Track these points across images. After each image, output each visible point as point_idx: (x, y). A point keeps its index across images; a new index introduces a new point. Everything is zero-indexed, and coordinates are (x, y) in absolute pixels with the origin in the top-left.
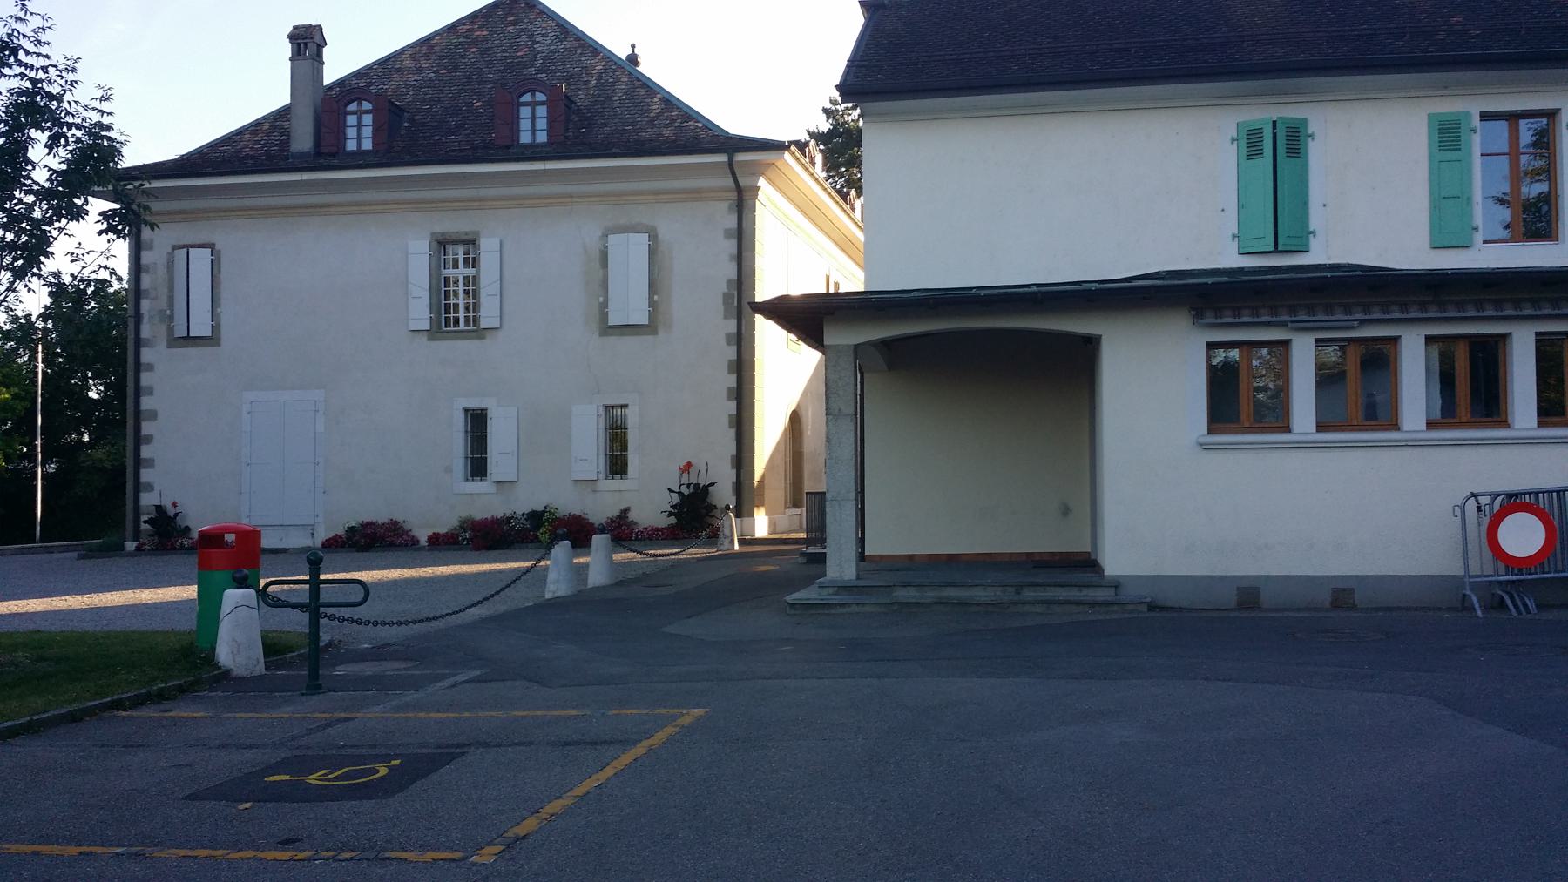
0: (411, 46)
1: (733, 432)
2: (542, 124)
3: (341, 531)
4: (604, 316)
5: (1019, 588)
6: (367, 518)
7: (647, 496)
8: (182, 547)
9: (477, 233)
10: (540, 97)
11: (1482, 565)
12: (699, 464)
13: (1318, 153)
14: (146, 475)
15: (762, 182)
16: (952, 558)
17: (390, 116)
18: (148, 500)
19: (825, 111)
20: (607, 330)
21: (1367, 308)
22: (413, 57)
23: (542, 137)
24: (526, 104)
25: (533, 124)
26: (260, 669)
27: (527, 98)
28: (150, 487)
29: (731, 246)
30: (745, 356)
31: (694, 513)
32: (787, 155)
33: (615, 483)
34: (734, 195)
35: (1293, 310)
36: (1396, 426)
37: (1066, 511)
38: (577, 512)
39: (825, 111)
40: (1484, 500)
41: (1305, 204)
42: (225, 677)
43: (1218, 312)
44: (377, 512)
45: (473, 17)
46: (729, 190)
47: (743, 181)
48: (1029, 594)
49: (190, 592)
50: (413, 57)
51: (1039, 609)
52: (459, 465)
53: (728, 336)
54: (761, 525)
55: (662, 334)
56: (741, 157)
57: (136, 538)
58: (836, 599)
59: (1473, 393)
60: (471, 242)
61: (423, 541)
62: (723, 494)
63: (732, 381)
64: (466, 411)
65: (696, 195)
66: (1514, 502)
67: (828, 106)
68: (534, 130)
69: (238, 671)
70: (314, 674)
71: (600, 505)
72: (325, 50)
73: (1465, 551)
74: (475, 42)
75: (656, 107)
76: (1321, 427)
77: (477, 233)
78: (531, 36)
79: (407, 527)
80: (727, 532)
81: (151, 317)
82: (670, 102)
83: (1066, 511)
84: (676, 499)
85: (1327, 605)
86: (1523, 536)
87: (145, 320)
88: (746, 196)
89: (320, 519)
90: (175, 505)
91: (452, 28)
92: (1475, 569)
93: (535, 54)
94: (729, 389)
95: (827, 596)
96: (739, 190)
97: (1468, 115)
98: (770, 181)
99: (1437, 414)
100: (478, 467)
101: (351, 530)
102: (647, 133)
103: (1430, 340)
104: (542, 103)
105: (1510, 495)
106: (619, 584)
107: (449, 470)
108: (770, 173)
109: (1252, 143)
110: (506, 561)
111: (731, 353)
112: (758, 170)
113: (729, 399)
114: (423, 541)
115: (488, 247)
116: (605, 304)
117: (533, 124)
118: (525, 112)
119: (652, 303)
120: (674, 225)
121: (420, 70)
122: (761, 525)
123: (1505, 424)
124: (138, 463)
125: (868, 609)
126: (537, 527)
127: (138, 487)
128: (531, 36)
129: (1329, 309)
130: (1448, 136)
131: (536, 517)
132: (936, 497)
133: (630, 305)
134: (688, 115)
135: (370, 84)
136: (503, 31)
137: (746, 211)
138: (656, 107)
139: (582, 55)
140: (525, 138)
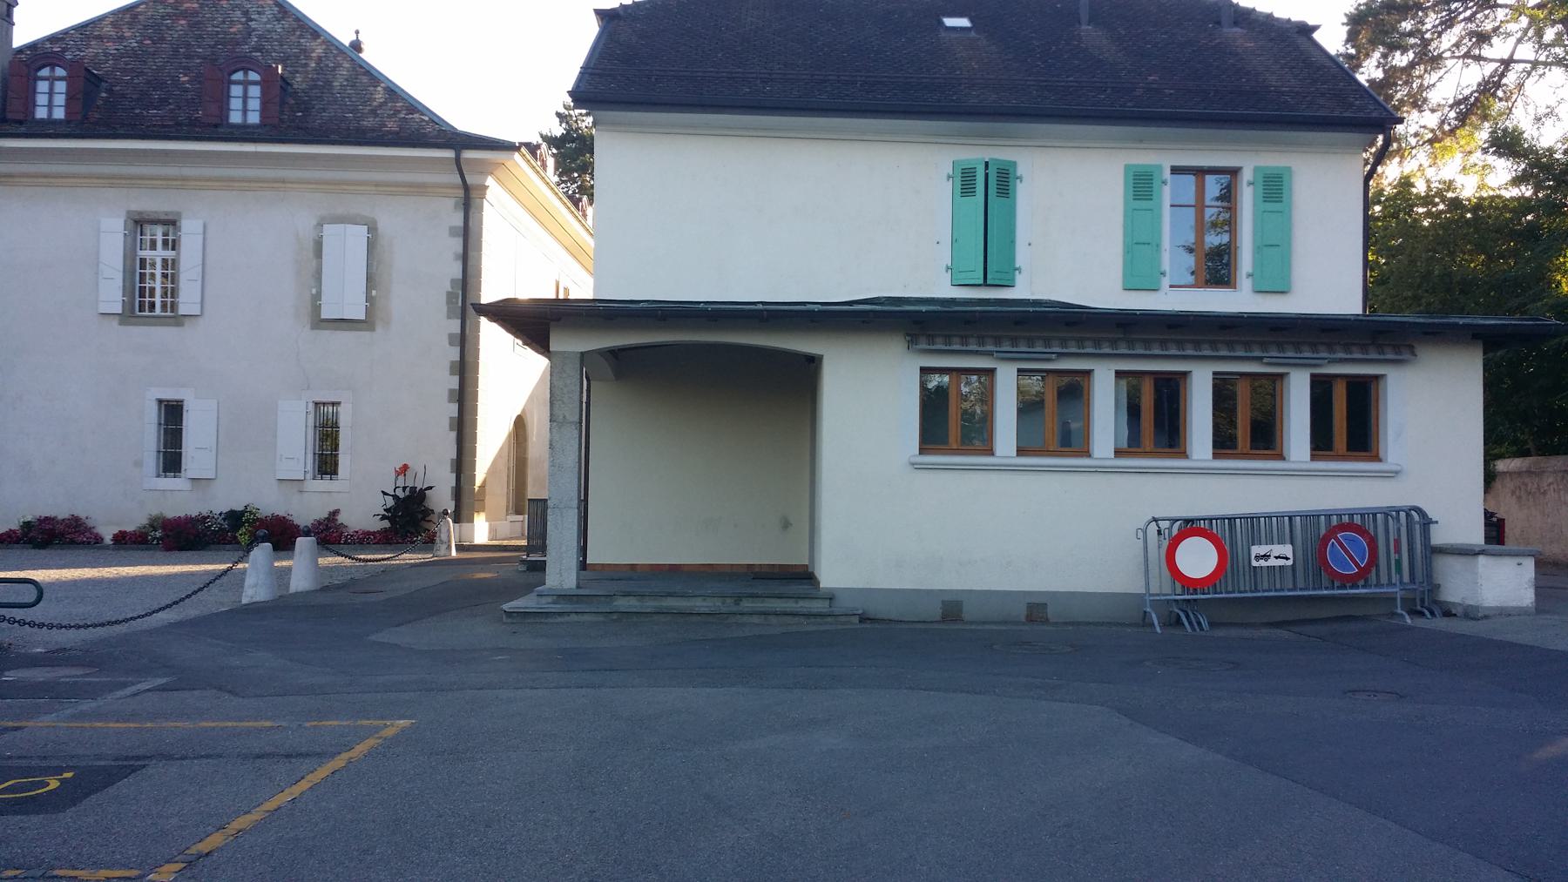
0: (114, 13)
1: (453, 435)
3: (15, 526)
4: (316, 309)
5: (738, 599)
9: (179, 214)
10: (253, 76)
11: (1162, 585)
12: (416, 466)
13: (1026, 195)
15: (490, 181)
16: (674, 570)
19: (558, 115)
20: (320, 323)
22: (114, 25)
24: (237, 83)
27: (239, 76)
29: (457, 244)
30: (469, 358)
31: (409, 517)
32: (517, 155)
33: (324, 484)
34: (461, 193)
35: (998, 341)
37: (786, 525)
38: (281, 513)
39: (558, 115)
40: (1164, 525)
41: (1013, 242)
43: (931, 339)
44: (59, 509)
46: (453, 187)
47: (469, 180)
48: (747, 605)
53: (451, 336)
54: (481, 531)
55: (379, 329)
56: (468, 154)
59: (1156, 424)
60: (171, 223)
61: (108, 539)
62: (441, 498)
63: (454, 382)
64: (160, 401)
65: (420, 189)
66: (1190, 527)
71: (307, 507)
72: (16, 10)
73: (1147, 571)
74: (185, 14)
75: (380, 96)
76: (1021, 451)
77: (179, 214)
78: (246, 13)
79: (90, 523)
80: (444, 537)
83: (786, 525)
84: (390, 502)
85: (1023, 619)
86: (1198, 559)
88: (473, 194)
93: (249, 32)
94: (451, 391)
95: (546, 605)
96: (466, 187)
97: (1160, 167)
98: (499, 181)
99: (1124, 444)
100: (171, 462)
102: (369, 122)
103: (1119, 374)
104: (255, 83)
105: (1187, 521)
107: (138, 464)
108: (499, 173)
109: (966, 181)
112: (486, 169)
113: (450, 401)
114: (108, 539)
115: (190, 230)
118: (236, 90)
119: (369, 298)
120: (394, 218)
121: (122, 38)
125: (586, 618)
128: (246, 13)
130: (1141, 186)
134: (413, 107)
135: (64, 50)
138: (380, 96)
139: (301, 36)
140: (235, 118)
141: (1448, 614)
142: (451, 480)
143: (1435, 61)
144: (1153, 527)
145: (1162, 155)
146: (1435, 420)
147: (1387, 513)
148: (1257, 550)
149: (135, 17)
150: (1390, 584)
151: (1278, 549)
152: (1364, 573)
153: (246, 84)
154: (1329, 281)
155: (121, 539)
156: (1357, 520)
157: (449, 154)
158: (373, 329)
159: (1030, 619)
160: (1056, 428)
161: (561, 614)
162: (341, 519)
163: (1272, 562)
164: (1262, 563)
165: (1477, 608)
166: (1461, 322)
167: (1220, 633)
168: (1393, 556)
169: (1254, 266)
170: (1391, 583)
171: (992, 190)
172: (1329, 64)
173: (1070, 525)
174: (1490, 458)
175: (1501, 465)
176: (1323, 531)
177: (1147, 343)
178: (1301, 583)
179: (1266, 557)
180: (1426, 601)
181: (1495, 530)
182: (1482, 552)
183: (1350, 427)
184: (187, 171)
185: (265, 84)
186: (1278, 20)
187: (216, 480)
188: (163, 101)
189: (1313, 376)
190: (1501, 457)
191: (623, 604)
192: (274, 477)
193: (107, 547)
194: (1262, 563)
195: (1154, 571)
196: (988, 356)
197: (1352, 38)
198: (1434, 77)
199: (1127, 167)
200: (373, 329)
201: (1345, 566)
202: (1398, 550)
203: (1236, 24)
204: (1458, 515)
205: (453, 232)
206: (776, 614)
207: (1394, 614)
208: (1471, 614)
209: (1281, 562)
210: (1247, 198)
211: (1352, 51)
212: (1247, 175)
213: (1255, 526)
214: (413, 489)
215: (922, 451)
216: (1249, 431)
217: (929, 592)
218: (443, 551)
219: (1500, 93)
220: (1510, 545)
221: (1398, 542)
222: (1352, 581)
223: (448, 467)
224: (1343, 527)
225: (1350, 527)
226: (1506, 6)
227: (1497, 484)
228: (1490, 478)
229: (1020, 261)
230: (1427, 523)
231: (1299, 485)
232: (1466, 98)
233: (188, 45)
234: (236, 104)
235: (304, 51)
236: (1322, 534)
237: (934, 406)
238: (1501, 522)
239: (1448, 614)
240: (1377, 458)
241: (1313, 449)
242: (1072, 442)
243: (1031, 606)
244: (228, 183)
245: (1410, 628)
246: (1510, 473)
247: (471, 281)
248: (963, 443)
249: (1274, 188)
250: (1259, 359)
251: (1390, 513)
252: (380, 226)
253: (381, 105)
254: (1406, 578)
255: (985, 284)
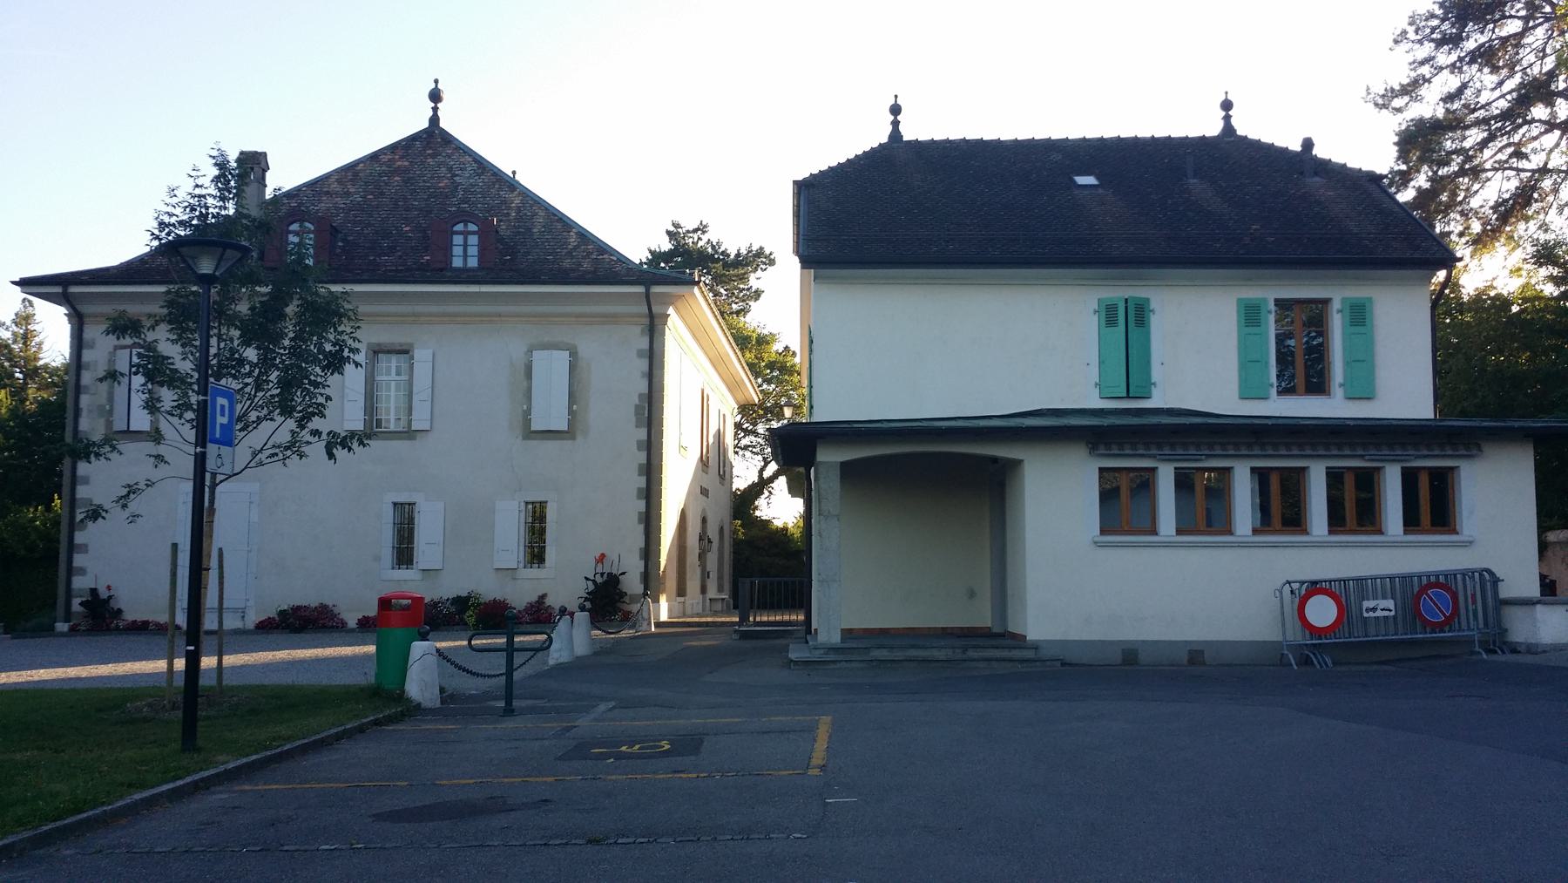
0: (337, 171)
1: (642, 527)
2: (473, 250)
3: (273, 614)
4: (527, 422)
5: (965, 649)
6: (297, 603)
7: (563, 579)
8: (117, 628)
9: (411, 345)
10: (472, 227)
11: (1295, 635)
12: (612, 556)
13: (1158, 324)
14: (79, 560)
15: (671, 311)
16: (884, 632)
17: (329, 232)
18: (79, 583)
19: (668, 232)
20: (530, 434)
21: (1211, 447)
22: (339, 181)
23: (473, 263)
24: (458, 233)
25: (465, 251)
26: (438, 704)
27: (460, 227)
28: (82, 571)
29: (643, 365)
30: (654, 462)
31: (607, 600)
32: (696, 289)
33: (534, 572)
34: (646, 321)
35: (1160, 446)
36: (1230, 533)
37: (972, 594)
38: (499, 597)
39: (668, 232)
40: (1296, 586)
41: (1148, 362)
42: (413, 711)
43: (1108, 445)
44: (308, 597)
45: (393, 148)
46: (639, 315)
47: (655, 309)
48: (972, 653)
49: (372, 649)
50: (339, 181)
51: (982, 665)
52: (387, 554)
53: (639, 443)
54: (664, 610)
55: (579, 439)
56: (656, 289)
57: (67, 620)
58: (832, 657)
59: (1282, 511)
60: (404, 351)
61: (352, 624)
62: (632, 583)
63: (642, 482)
64: (395, 504)
65: (612, 319)
66: (1316, 587)
67: (672, 229)
68: (465, 256)
69: (427, 704)
70: (509, 702)
71: (519, 595)
72: (268, 174)
73: (1283, 625)
74: (397, 171)
75: (573, 240)
76: (1179, 532)
77: (411, 345)
78: (450, 169)
79: (336, 611)
80: (645, 615)
81: (90, 411)
82: (585, 236)
83: (972, 594)
84: (591, 587)
85: (1185, 661)
86: (1322, 612)
87: (84, 414)
88: (657, 321)
89: (251, 603)
90: (109, 588)
91: (374, 157)
92: (1290, 637)
93: (456, 186)
94: (639, 490)
95: (816, 655)
96: (651, 316)
97: (1265, 300)
98: (677, 310)
99: (1258, 524)
100: (404, 555)
101: (282, 613)
102: (567, 263)
103: (1253, 470)
104: (473, 233)
105: (1314, 583)
106: (596, 654)
107: (377, 559)
108: (679, 304)
109: (1109, 315)
110: (135, 677)
111: (642, 457)
112: (669, 300)
113: (639, 498)
114: (352, 624)
115: (421, 355)
116: (528, 412)
117: (465, 251)
118: (458, 239)
119: (571, 412)
120: (590, 344)
121: (348, 194)
122: (664, 610)
123: (1305, 532)
124: (72, 548)
125: (854, 665)
126: (462, 611)
127: (70, 571)
128: (450, 169)
129: (1185, 446)
130: (1250, 315)
131: (462, 603)
132: (866, 584)
133: (551, 411)
134: (603, 249)
135: (300, 205)
136: (423, 163)
137: (656, 335)
138: (573, 240)
139: (500, 189)
140: (457, 262)
141: (1514, 651)
142: (640, 566)
143: (1476, 173)
144: (1287, 589)
145: (1269, 291)
146: (1497, 499)
147: (1464, 573)
148: (1367, 604)
149: (356, 174)
150: (1469, 629)
151: (1383, 603)
152: (1449, 621)
153: (466, 234)
154: (1405, 388)
155: (265, 627)
156: (1442, 579)
157: (640, 289)
158: (573, 438)
159: (1192, 662)
160: (1205, 513)
161: (834, 662)
162: (548, 602)
163: (1379, 613)
164: (1371, 614)
165: (1537, 645)
166: (1516, 425)
167: (1339, 668)
168: (1471, 607)
169: (1345, 377)
170: (1471, 627)
171: (1130, 322)
172: (1397, 209)
173: (1221, 588)
174: (1542, 529)
175: (1551, 537)
176: (1416, 589)
177: (1275, 446)
178: (1401, 630)
179: (1374, 609)
180: (1497, 641)
181: (1549, 588)
182: (1539, 602)
183: (1433, 508)
184: (419, 308)
185: (481, 234)
186: (1351, 169)
187: (443, 570)
188: (392, 249)
189: (1403, 468)
190: (1551, 529)
191: (876, 654)
192: (486, 565)
193: (352, 630)
194: (1371, 614)
195: (1288, 625)
196: (1146, 456)
197: (1403, 155)
198: (1476, 187)
199: (1239, 301)
200: (573, 438)
201: (1435, 615)
202: (1474, 602)
203: (1316, 174)
204: (1519, 572)
205: (640, 354)
206: (997, 660)
207: (1473, 653)
208: (1532, 649)
209: (1386, 613)
210: (1337, 324)
211: (1404, 167)
212: (1336, 305)
213: (1363, 586)
214: (610, 574)
215: (1103, 532)
216: (1355, 511)
217: (1112, 643)
218: (645, 626)
219: (1536, 195)
220: (1560, 597)
221: (1474, 596)
222: (1440, 627)
223: (637, 556)
224: (1430, 585)
225: (1437, 585)
226: (1540, 121)
227: (1549, 553)
228: (1543, 547)
229: (1155, 377)
230: (1496, 581)
231: (1394, 554)
232: (1506, 201)
233: (405, 199)
234: (457, 251)
235: (504, 202)
236: (1415, 592)
237: (1108, 496)
238: (1553, 582)
239: (1514, 651)
240: (1454, 532)
241: (1330, 524)
242: (1294, 520)
243: (1190, 652)
244: (453, 317)
245: (1485, 661)
246: (1559, 543)
247: (655, 395)
248: (1360, 524)
249: (1359, 315)
250: (1362, 457)
251: (1467, 574)
252: (580, 350)
253: (576, 248)
254: (1481, 625)
255: (1128, 397)
